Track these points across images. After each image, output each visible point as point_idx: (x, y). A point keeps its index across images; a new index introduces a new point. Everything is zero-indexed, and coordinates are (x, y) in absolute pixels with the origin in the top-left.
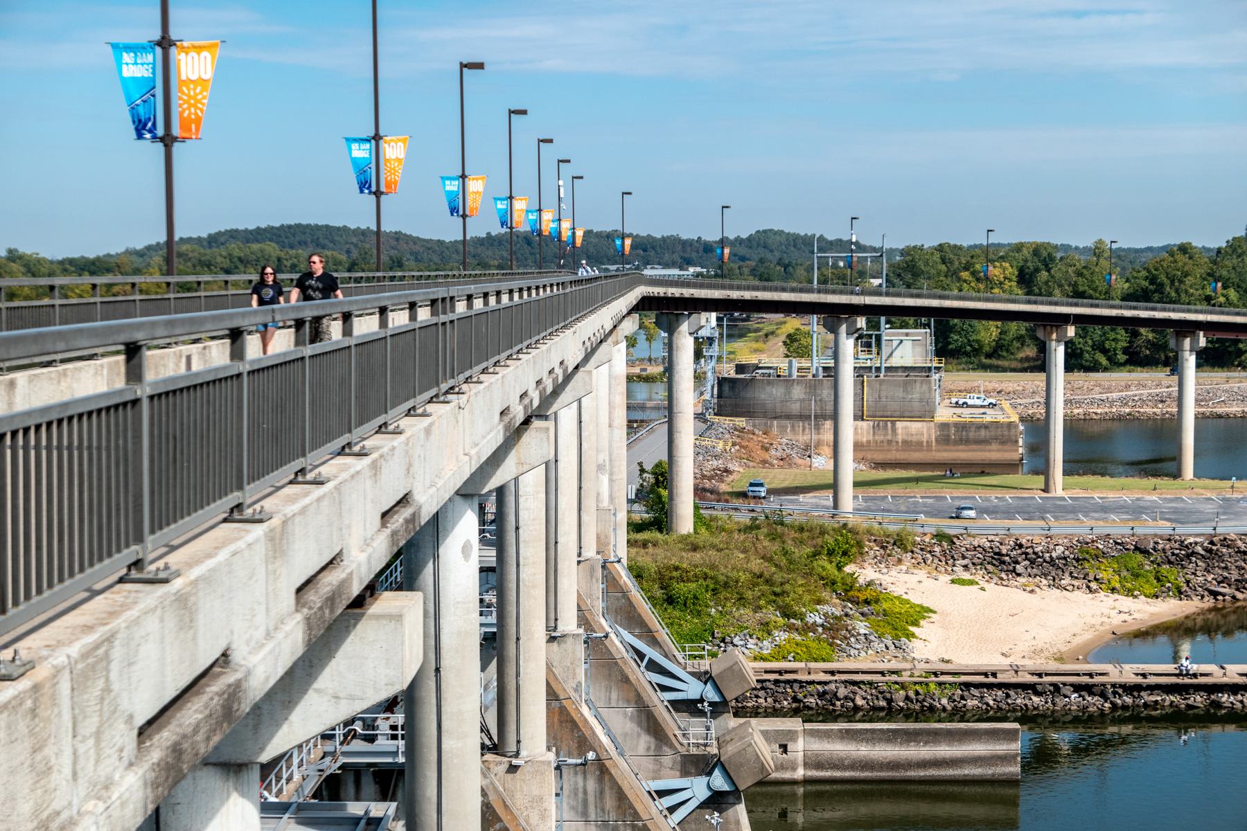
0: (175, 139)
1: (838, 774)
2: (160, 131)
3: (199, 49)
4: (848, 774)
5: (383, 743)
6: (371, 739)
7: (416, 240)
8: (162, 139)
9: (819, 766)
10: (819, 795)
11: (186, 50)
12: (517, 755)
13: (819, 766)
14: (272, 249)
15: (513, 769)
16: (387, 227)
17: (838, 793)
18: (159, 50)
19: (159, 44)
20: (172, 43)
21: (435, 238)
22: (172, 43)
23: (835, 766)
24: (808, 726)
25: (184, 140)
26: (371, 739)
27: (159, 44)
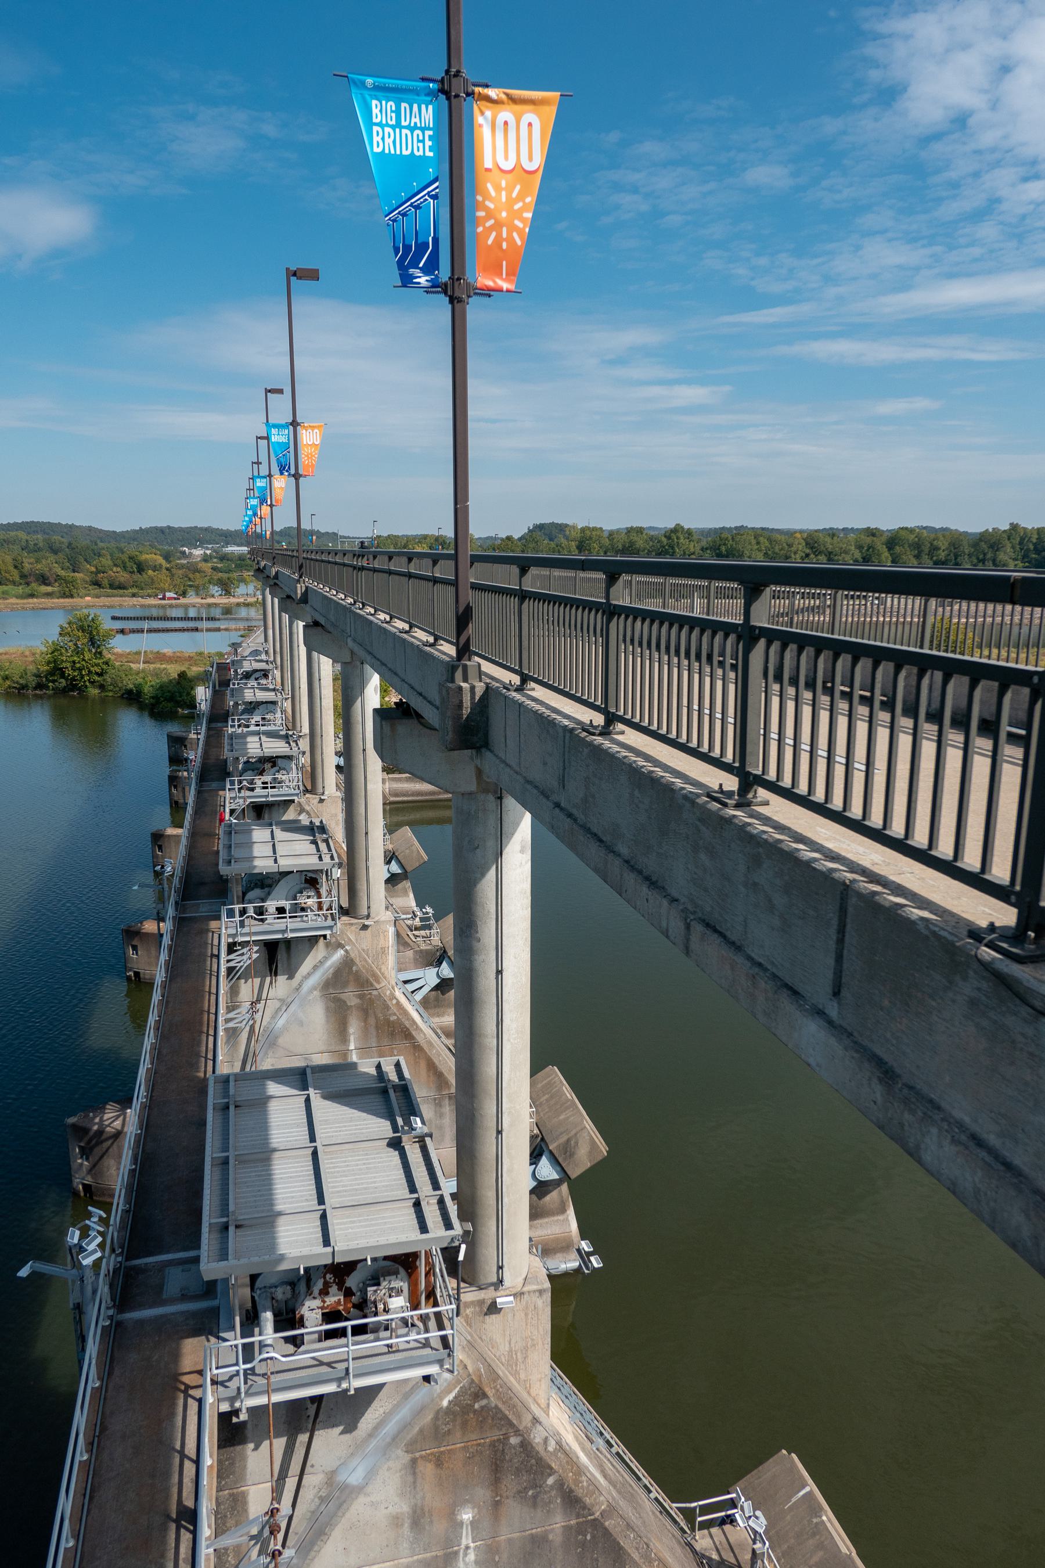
0: (301, 476)
1: (405, 799)
2: (293, 472)
3: (313, 428)
4: (410, 798)
5: (259, 791)
6: (252, 790)
7: (101, 531)
8: (293, 476)
9: (396, 795)
10: (397, 810)
11: (306, 428)
12: (323, 794)
13: (396, 795)
14: (22, 535)
15: (321, 801)
16: (305, 525)
17: (404, 808)
18: (291, 427)
19: (291, 424)
20: (298, 424)
21: (111, 530)
22: (298, 424)
23: (404, 795)
24: (391, 776)
25: (305, 476)
26: (252, 790)
27: (291, 424)
